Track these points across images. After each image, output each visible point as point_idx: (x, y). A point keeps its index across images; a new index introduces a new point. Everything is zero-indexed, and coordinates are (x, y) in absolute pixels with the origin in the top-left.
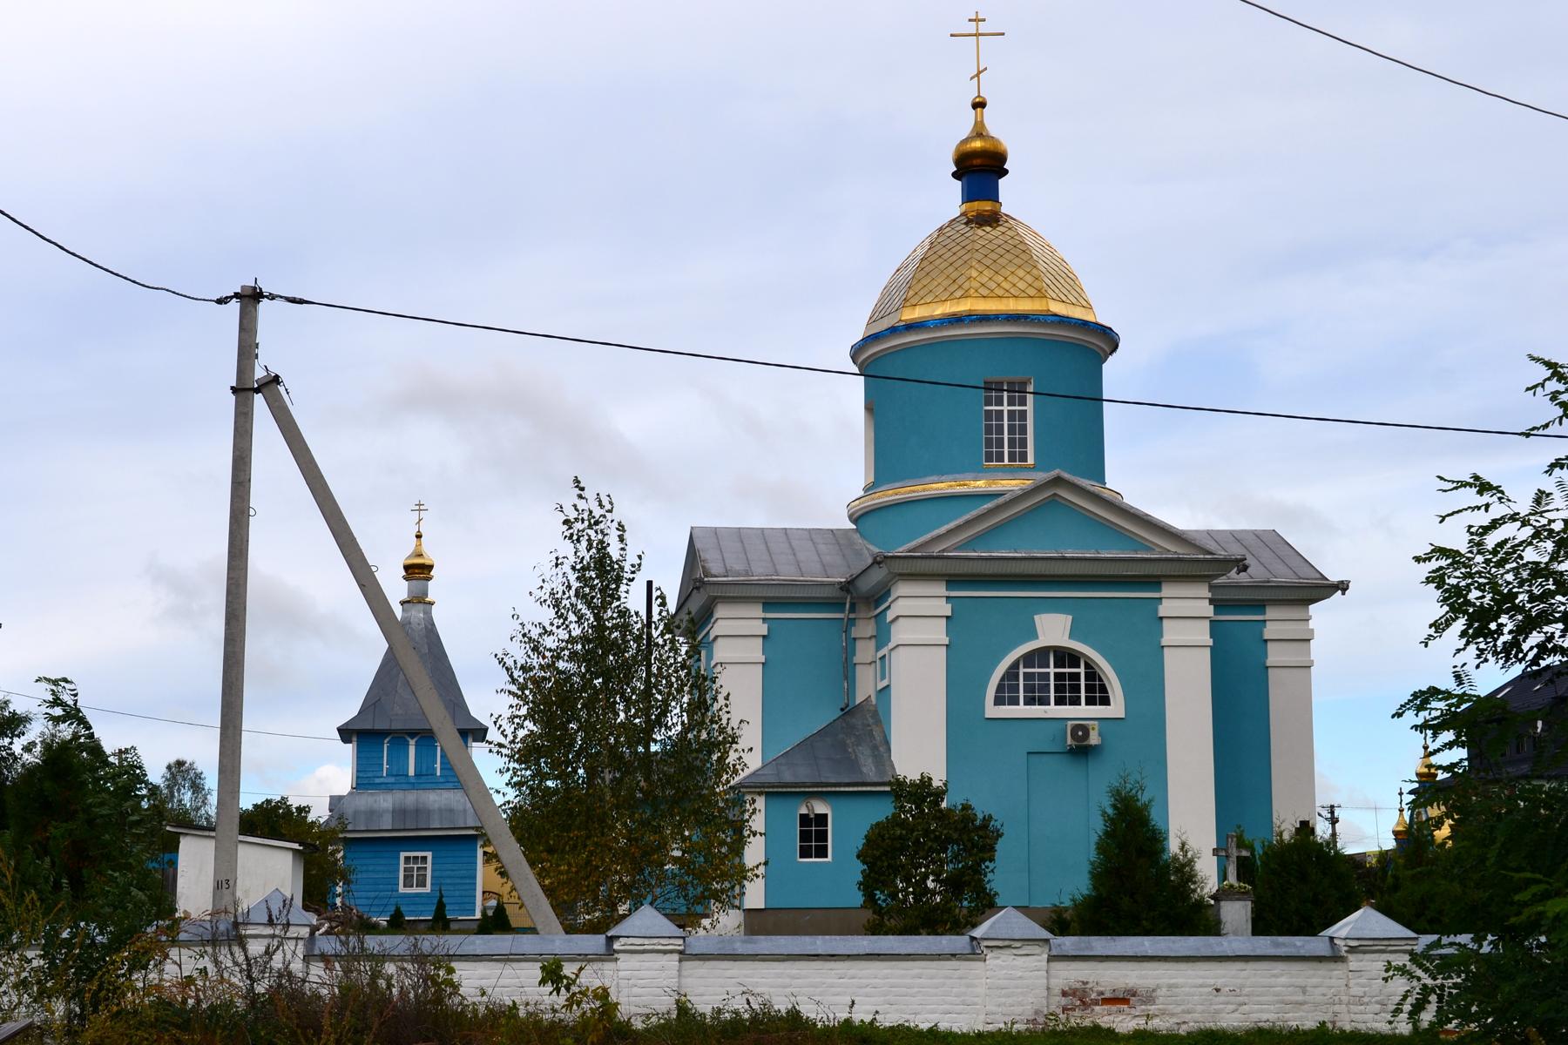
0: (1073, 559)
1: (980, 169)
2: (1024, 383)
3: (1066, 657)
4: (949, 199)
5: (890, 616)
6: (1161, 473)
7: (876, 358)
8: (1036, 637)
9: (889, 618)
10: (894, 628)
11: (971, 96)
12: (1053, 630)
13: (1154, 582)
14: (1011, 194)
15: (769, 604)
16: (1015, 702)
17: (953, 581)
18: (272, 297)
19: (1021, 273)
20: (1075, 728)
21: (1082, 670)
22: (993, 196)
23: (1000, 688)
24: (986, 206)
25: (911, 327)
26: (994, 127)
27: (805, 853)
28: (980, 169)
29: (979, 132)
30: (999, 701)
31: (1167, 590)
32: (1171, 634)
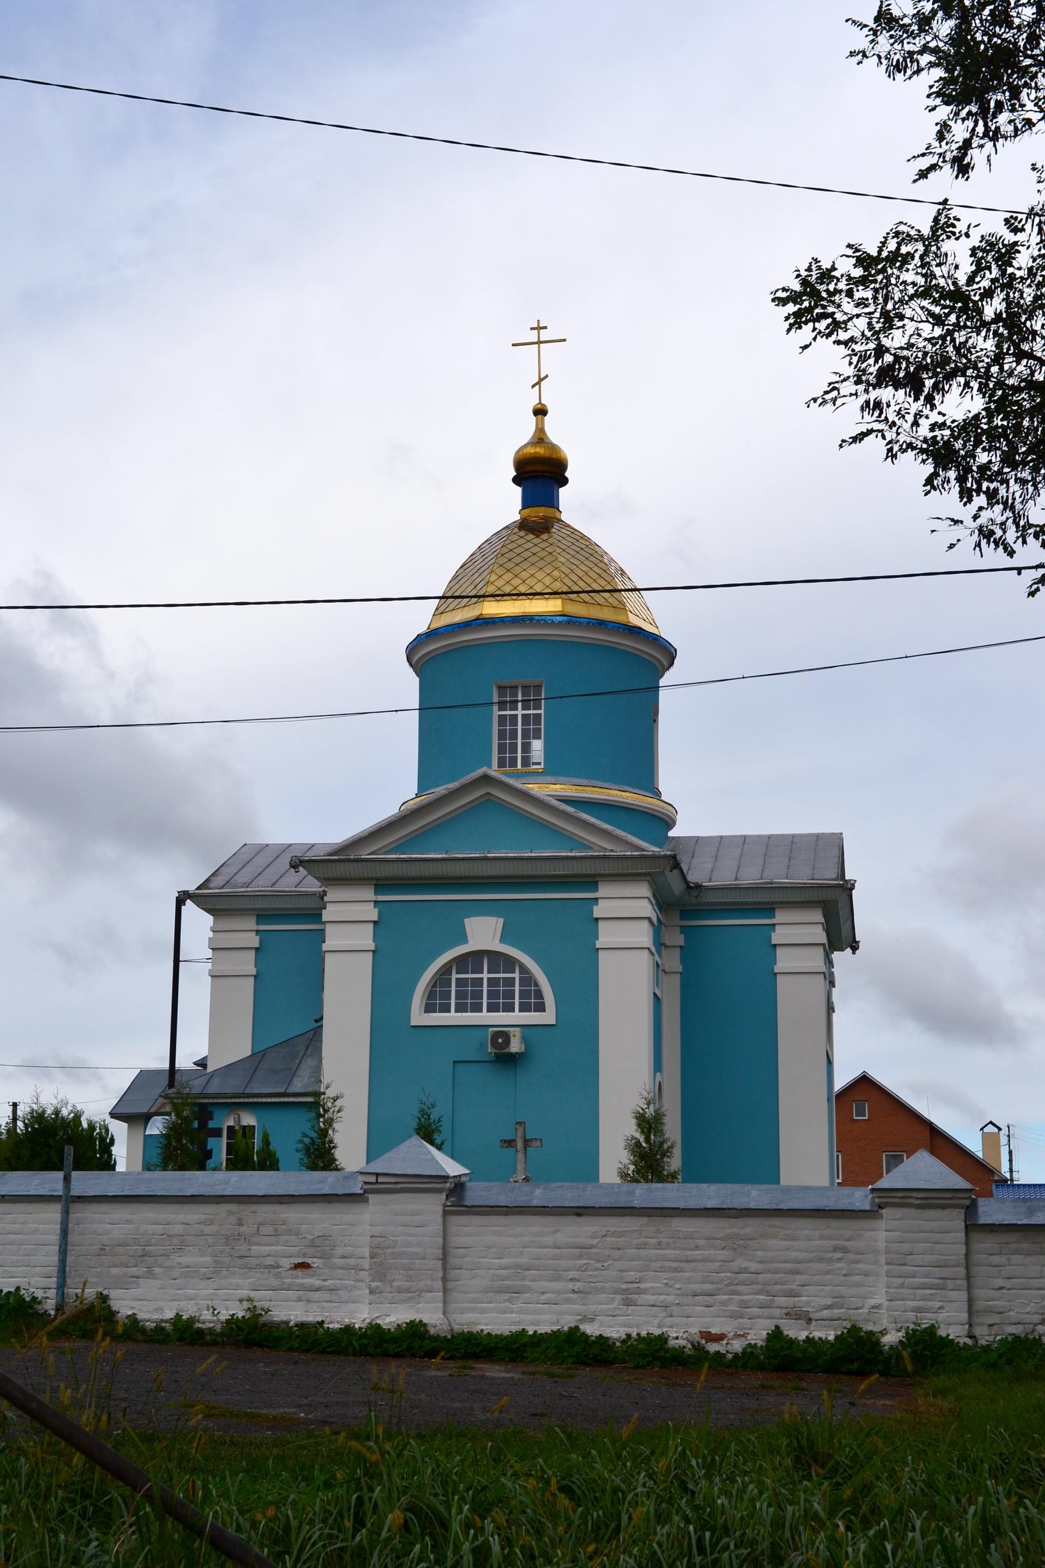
0: (496, 859)
1: (541, 473)
2: (539, 687)
3: (498, 960)
4: (507, 504)
6: (717, 781)
8: (464, 940)
12: (484, 933)
13: (590, 882)
14: (572, 503)
15: (263, 916)
16: (477, 1008)
17: (382, 885)
19: (540, 575)
20: (496, 1035)
21: (516, 975)
22: (552, 502)
23: (431, 995)
24: (541, 512)
26: (553, 434)
28: (541, 473)
29: (540, 438)
30: (429, 1008)
31: (604, 890)
32: (607, 936)
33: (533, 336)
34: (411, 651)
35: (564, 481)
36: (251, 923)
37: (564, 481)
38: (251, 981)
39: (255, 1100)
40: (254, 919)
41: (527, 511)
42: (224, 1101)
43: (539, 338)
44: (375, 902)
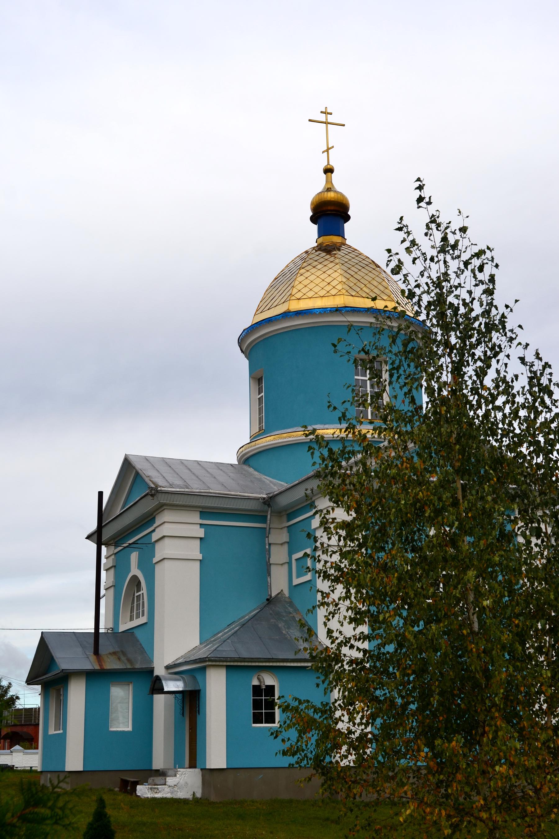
4: (310, 235)
5: (155, 537)
7: (265, 339)
9: (154, 539)
10: (158, 546)
11: (323, 164)
15: (205, 513)
18: (328, 162)
22: (340, 233)
24: (336, 239)
25: (299, 313)
27: (257, 719)
33: (322, 118)
34: (241, 341)
35: (347, 218)
36: (195, 518)
37: (347, 218)
38: (197, 566)
39: (282, 664)
40: (198, 515)
41: (321, 239)
42: (257, 664)
43: (326, 119)
44: (201, 524)
